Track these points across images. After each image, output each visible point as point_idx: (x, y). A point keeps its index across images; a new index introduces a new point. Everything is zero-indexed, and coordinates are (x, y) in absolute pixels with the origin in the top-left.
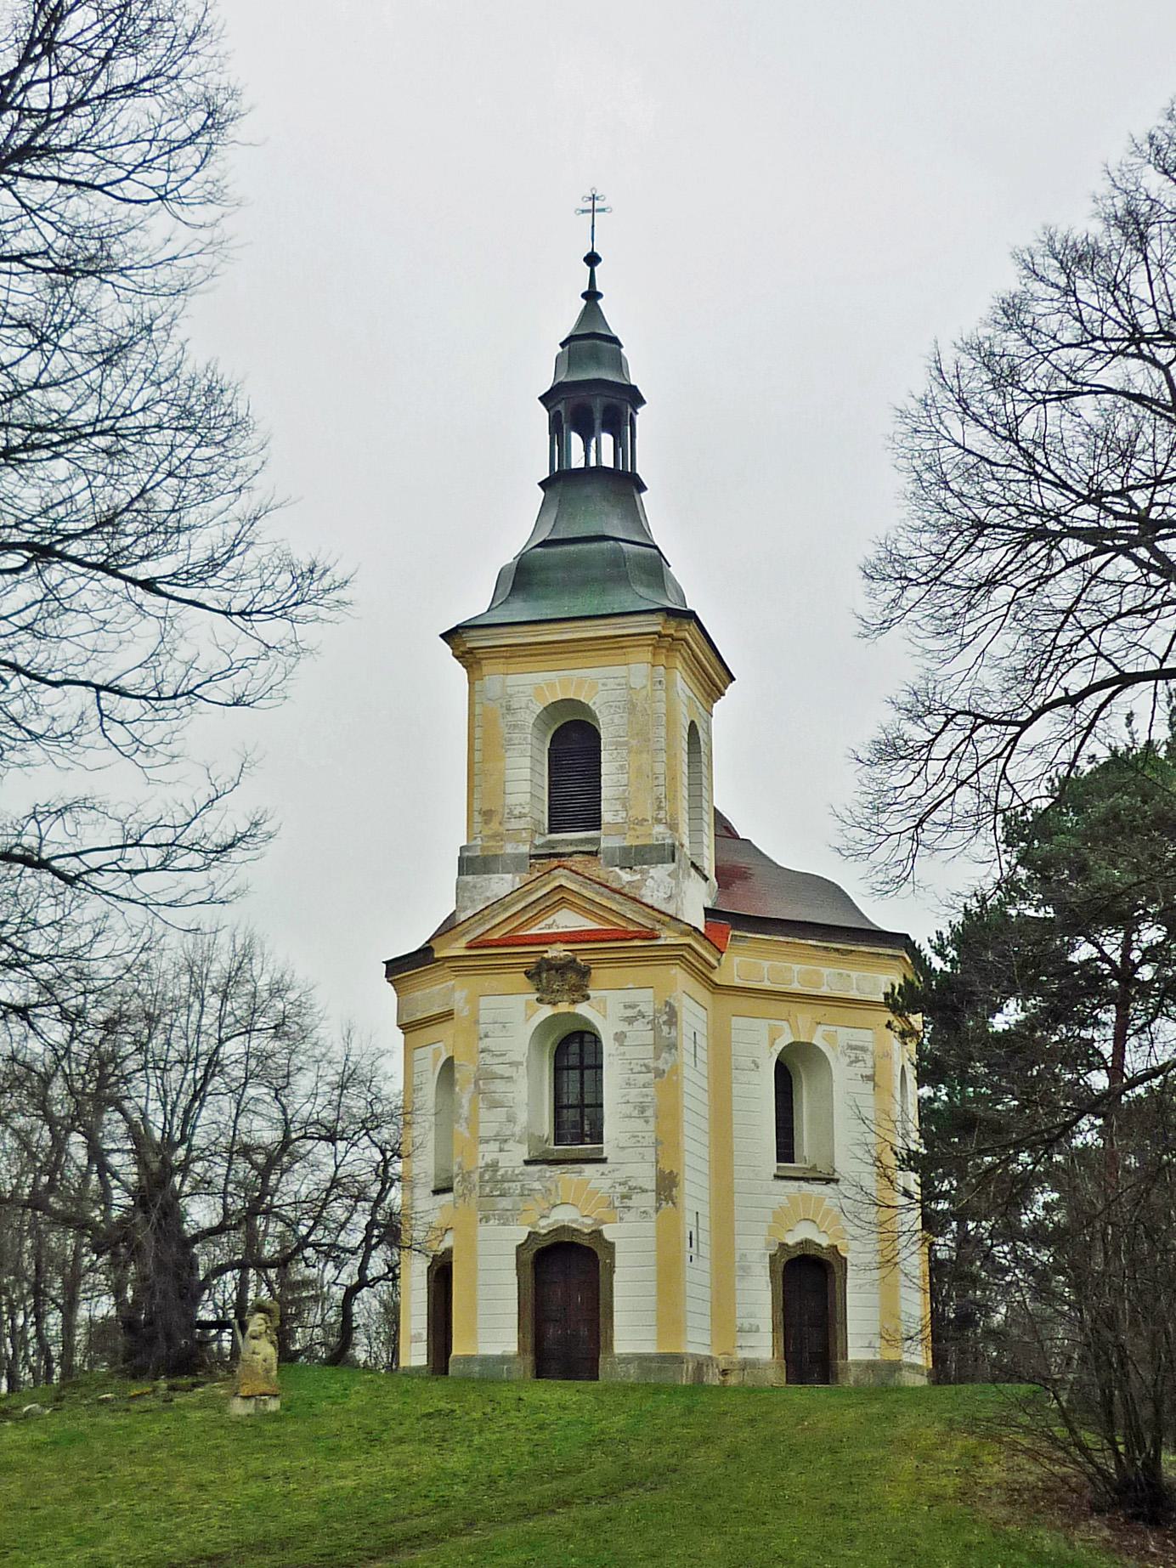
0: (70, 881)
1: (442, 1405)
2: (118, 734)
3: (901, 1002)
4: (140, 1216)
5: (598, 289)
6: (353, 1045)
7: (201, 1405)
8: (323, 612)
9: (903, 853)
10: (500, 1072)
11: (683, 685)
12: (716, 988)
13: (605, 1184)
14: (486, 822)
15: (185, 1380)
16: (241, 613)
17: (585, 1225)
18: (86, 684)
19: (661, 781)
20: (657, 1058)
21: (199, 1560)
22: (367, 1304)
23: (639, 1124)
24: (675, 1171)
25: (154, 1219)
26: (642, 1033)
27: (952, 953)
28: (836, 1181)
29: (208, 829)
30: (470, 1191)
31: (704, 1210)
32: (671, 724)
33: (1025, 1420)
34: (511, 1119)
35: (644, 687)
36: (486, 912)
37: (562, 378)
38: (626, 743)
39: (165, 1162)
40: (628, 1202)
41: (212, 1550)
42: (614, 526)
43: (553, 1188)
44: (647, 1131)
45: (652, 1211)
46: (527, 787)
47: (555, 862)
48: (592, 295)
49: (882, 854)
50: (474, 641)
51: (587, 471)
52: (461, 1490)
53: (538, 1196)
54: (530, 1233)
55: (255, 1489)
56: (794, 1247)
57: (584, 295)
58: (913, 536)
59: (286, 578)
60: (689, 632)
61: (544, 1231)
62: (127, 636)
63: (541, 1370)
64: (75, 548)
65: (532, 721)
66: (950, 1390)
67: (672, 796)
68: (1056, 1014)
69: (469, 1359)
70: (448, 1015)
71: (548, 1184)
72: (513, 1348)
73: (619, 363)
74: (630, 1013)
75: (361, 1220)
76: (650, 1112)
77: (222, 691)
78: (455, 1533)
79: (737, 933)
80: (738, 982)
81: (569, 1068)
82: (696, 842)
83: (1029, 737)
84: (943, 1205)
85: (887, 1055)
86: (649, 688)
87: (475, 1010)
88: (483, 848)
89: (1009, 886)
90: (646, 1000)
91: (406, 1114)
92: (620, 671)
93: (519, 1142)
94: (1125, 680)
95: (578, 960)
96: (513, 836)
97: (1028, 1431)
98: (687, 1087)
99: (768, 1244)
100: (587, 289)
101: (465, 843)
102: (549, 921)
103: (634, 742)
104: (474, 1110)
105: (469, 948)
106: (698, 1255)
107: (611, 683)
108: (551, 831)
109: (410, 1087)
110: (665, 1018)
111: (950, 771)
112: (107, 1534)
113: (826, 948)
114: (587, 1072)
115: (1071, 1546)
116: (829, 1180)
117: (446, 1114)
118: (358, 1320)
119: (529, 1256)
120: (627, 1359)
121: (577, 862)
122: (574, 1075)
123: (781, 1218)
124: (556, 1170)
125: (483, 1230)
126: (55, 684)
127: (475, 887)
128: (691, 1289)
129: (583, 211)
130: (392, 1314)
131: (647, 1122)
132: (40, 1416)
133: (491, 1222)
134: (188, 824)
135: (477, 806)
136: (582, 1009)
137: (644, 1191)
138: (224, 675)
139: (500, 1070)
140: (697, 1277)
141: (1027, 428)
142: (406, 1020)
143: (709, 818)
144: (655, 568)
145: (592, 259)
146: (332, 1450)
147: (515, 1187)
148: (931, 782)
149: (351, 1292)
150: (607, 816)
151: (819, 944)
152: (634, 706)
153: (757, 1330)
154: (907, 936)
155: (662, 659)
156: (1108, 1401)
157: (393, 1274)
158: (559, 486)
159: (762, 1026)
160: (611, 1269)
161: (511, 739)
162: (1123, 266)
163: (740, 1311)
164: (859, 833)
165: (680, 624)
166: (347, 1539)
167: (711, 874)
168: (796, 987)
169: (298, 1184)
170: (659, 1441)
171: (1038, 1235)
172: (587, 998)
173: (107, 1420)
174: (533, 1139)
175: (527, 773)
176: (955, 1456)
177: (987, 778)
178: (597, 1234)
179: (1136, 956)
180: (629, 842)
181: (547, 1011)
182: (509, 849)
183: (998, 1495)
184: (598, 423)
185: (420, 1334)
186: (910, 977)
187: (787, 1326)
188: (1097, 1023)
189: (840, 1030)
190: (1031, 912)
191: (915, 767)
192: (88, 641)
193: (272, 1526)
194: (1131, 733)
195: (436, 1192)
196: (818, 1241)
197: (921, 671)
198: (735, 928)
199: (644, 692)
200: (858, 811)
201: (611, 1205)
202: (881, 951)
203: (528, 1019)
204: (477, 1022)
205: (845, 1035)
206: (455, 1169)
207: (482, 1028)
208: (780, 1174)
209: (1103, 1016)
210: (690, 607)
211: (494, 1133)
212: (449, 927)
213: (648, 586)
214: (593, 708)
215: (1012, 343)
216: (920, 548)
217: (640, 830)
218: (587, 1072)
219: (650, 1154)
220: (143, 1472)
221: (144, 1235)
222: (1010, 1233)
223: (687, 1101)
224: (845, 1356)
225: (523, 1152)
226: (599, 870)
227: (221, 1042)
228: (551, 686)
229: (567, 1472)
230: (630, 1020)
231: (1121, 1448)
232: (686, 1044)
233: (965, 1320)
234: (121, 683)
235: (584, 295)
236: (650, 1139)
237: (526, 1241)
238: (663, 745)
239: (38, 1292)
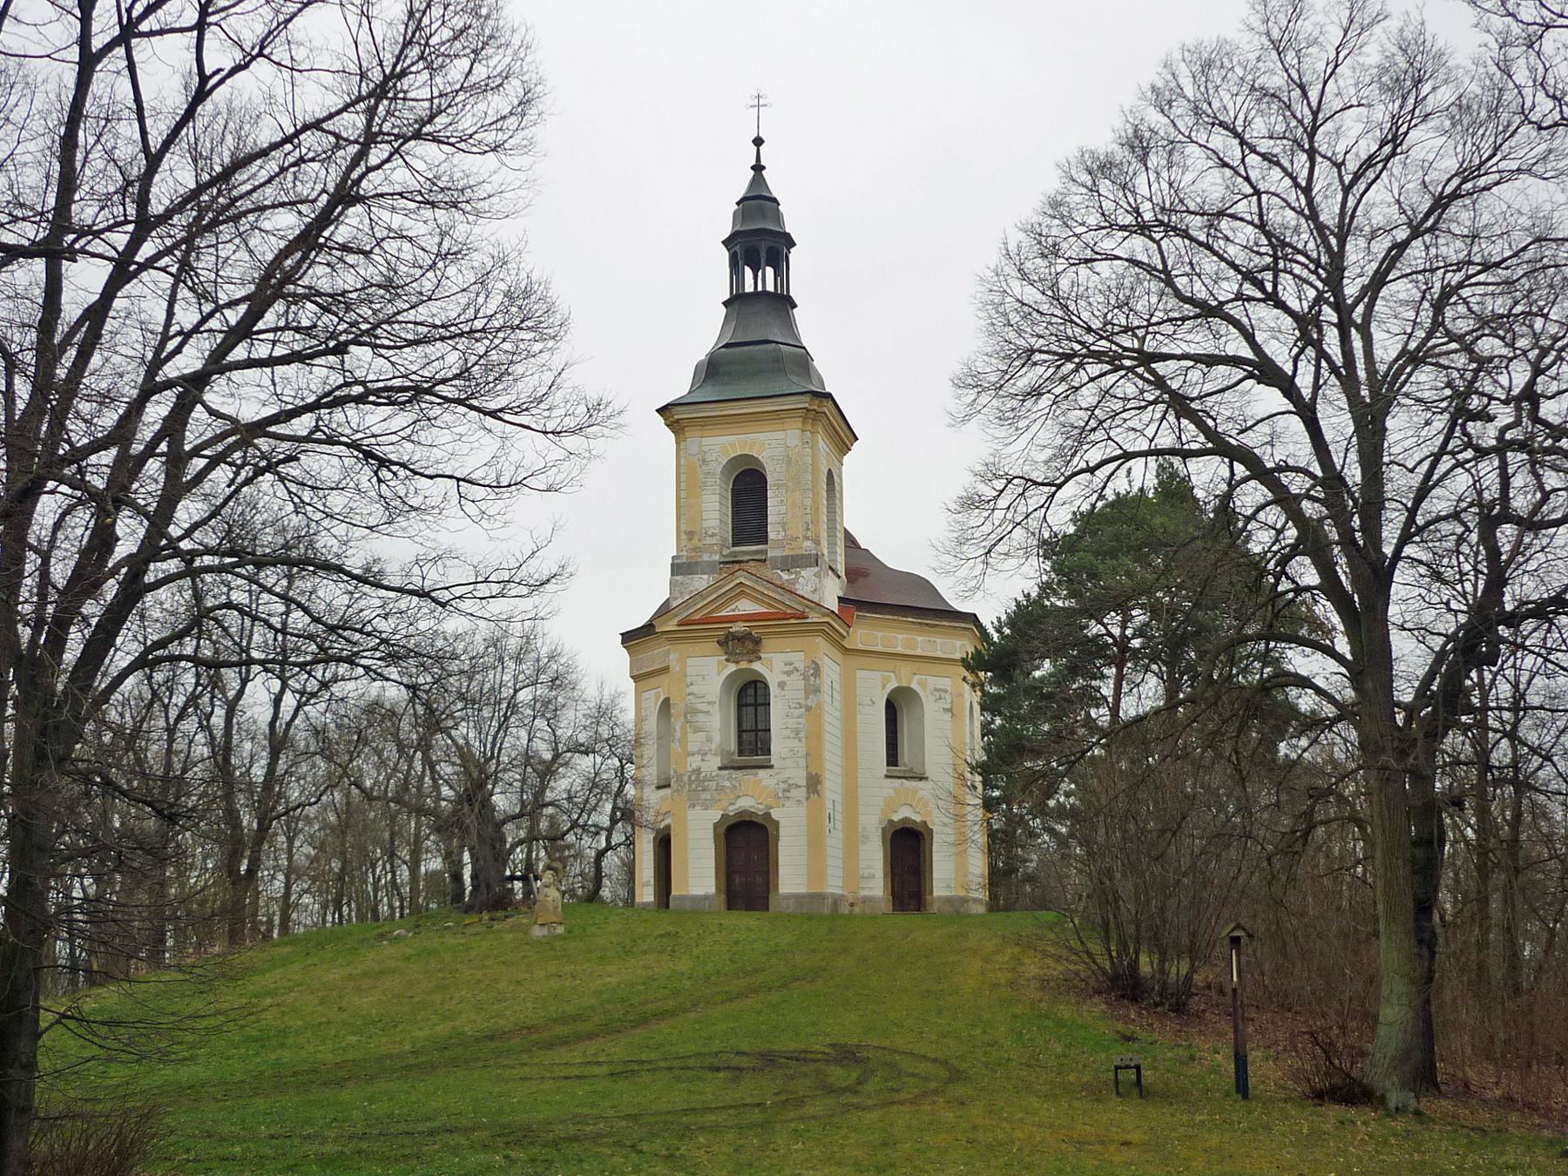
0: (443, 605)
1: (670, 929)
2: (470, 508)
3: (974, 664)
4: (466, 808)
5: (763, 163)
6: (605, 693)
7: (511, 930)
8: (606, 432)
9: (977, 571)
11: (823, 444)
12: (847, 651)
14: (690, 540)
15: (500, 914)
16: (552, 433)
17: (759, 809)
18: (451, 477)
20: (807, 698)
21: (522, 1028)
22: (611, 861)
23: (794, 743)
25: (476, 810)
26: (796, 682)
27: (1007, 631)
28: (926, 779)
29: (532, 570)
31: (839, 799)
32: (815, 471)
33: (1052, 936)
34: (709, 740)
38: (785, 485)
39: (482, 771)
40: (788, 794)
41: (529, 1023)
44: (801, 748)
45: (804, 800)
47: (737, 566)
48: (758, 168)
49: (963, 572)
50: (680, 414)
51: (756, 294)
52: (688, 984)
55: (554, 984)
57: (752, 168)
58: (986, 358)
59: (582, 409)
62: (476, 445)
63: (731, 906)
64: (442, 389)
66: (1002, 916)
67: (816, 521)
68: (1074, 670)
69: (682, 898)
70: (666, 670)
72: (713, 890)
73: (777, 217)
75: (608, 807)
76: (802, 735)
77: (539, 482)
78: (686, 1011)
80: (860, 647)
81: (747, 705)
82: (833, 552)
83: (1062, 494)
84: (996, 793)
85: (961, 695)
87: (684, 667)
89: (1046, 589)
90: (799, 660)
91: (638, 742)
92: (780, 435)
94: (1127, 456)
97: (1055, 944)
98: (827, 718)
102: (733, 607)
104: (684, 733)
108: (734, 545)
109: (640, 720)
111: (1009, 516)
112: (460, 1013)
115: (1081, 1015)
117: (665, 736)
118: (605, 871)
119: (722, 830)
120: (789, 897)
121: (751, 566)
122: (752, 709)
124: (740, 773)
126: (431, 477)
130: (630, 869)
132: (405, 937)
134: (519, 568)
136: (756, 666)
137: (798, 786)
138: (543, 470)
140: (834, 843)
141: (1064, 284)
142: (636, 673)
143: (840, 536)
144: (803, 362)
145: (758, 142)
146: (601, 958)
147: (713, 785)
148: (997, 524)
149: (600, 854)
150: (771, 535)
152: (789, 460)
153: (873, 877)
154: (975, 615)
156: (1106, 924)
157: (630, 843)
158: (737, 304)
159: (877, 676)
162: (1131, 173)
163: (862, 865)
164: (948, 558)
166: (616, 1016)
167: (843, 574)
168: (900, 650)
169: (560, 786)
170: (813, 951)
171: (1061, 813)
173: (450, 940)
174: (724, 753)
176: (1006, 959)
177: (1033, 524)
178: (767, 815)
179: (1129, 632)
181: (732, 668)
182: (706, 557)
183: (1034, 984)
184: (763, 260)
186: (979, 647)
187: (893, 874)
188: (1103, 677)
190: (1060, 604)
191: (986, 514)
192: (449, 448)
193: (567, 1008)
194: (1130, 482)
195: (658, 788)
197: (991, 451)
200: (947, 543)
201: (776, 796)
204: (685, 675)
205: (932, 682)
206: (672, 773)
207: (689, 680)
209: (1106, 671)
210: (828, 390)
212: (664, 610)
213: (798, 375)
215: (1055, 229)
216: (990, 369)
219: (802, 762)
220: (479, 974)
221: (470, 820)
222: (1040, 810)
223: (828, 727)
225: (717, 761)
226: (767, 572)
227: (516, 691)
228: (732, 445)
229: (755, 971)
231: (1114, 954)
232: (826, 688)
233: (1010, 870)
234: (473, 476)
235: (752, 168)
239: (392, 855)
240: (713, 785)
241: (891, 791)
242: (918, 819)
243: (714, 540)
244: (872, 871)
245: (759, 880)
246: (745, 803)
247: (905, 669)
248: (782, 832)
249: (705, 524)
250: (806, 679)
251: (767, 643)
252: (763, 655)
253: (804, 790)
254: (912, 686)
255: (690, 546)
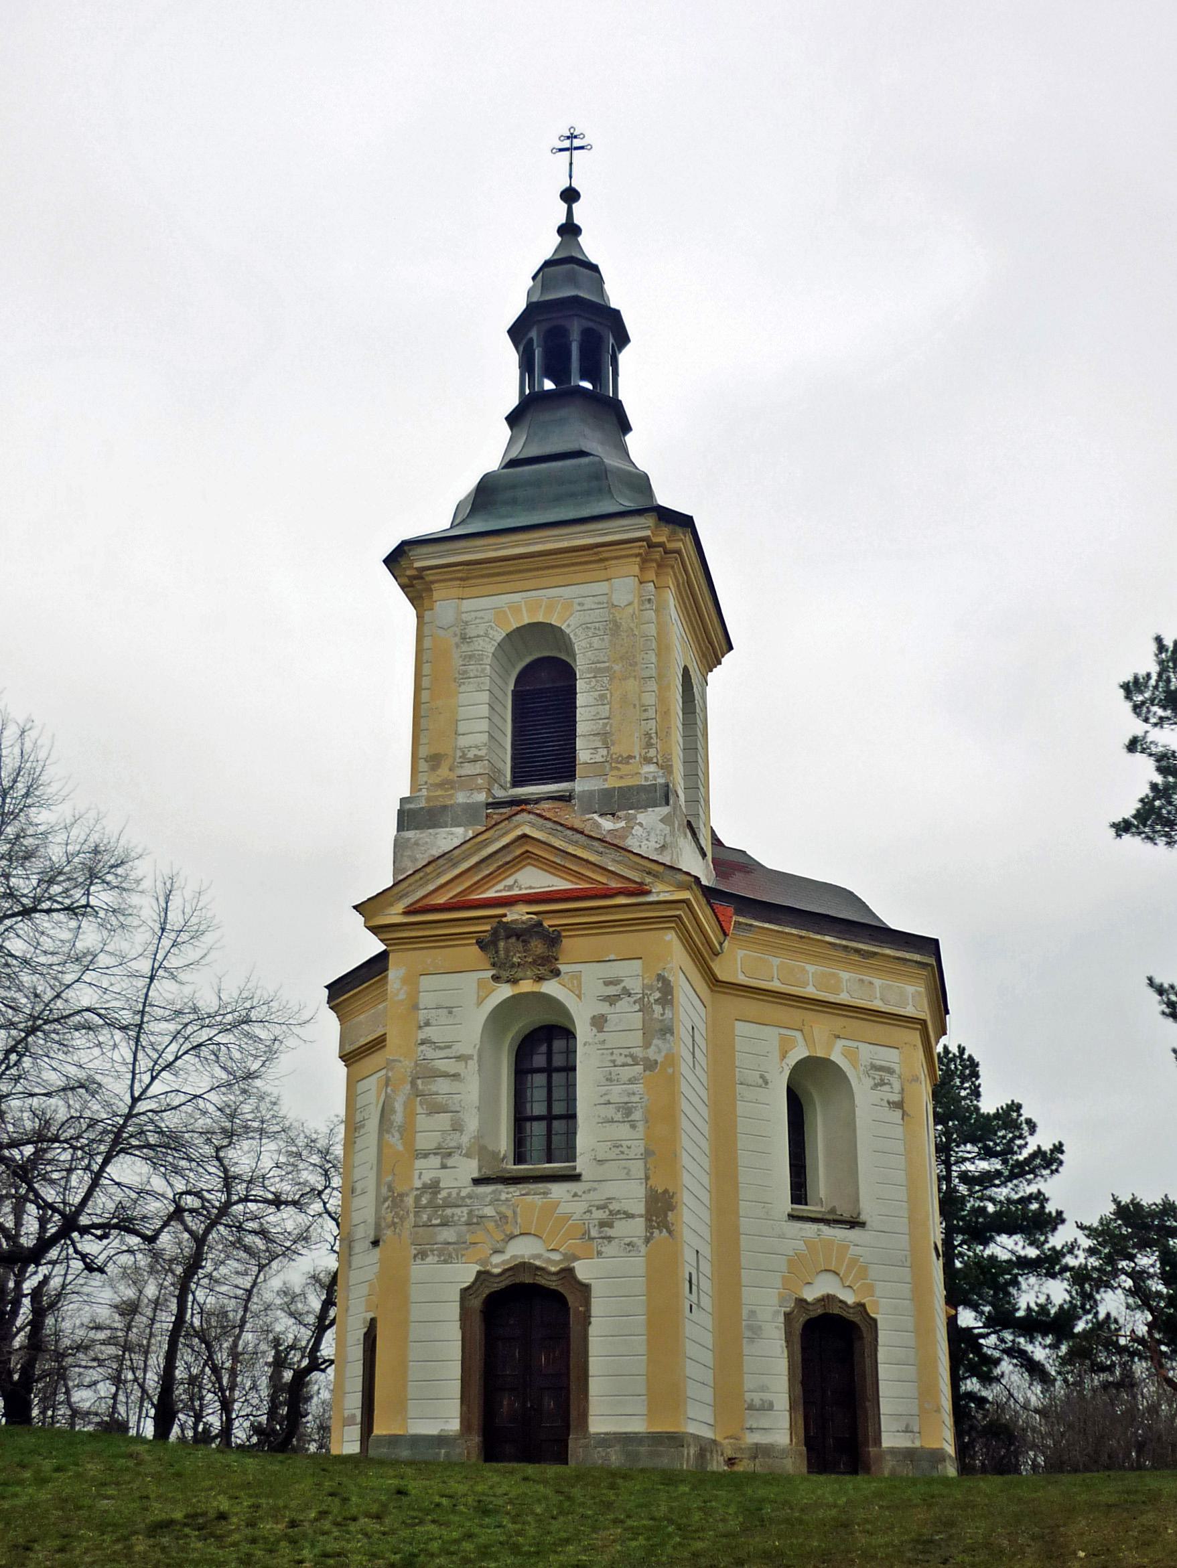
10: (443, 1069)
13: (578, 1208)
14: (434, 768)
17: (552, 1261)
19: (651, 714)
20: (647, 1045)
23: (623, 1131)
24: (671, 1191)
26: (627, 1015)
28: (862, 1225)
30: (402, 1219)
31: (706, 1251)
34: (457, 1127)
35: (630, 604)
36: (428, 869)
37: (534, 299)
38: (608, 669)
42: (594, 443)
43: (509, 1213)
44: (633, 1138)
45: (639, 1242)
46: (484, 725)
48: (569, 230)
53: (491, 1225)
54: (479, 1273)
56: (813, 1304)
60: (682, 543)
61: (497, 1271)
65: (493, 650)
71: (503, 1209)
72: (454, 1426)
74: (612, 990)
79: (741, 920)
80: (742, 979)
86: (636, 605)
88: (428, 799)
90: (632, 974)
92: (603, 587)
93: (468, 1155)
95: (546, 924)
96: (466, 782)
99: (782, 1300)
100: (564, 221)
101: (408, 794)
102: (510, 881)
103: (617, 667)
104: (410, 1115)
105: (408, 912)
106: (698, 1305)
107: (589, 604)
108: (516, 783)
110: (657, 995)
113: (846, 947)
114: (555, 1076)
116: (855, 1223)
119: (476, 1303)
120: (607, 1440)
123: (799, 1267)
124: (514, 1191)
125: (418, 1270)
127: (417, 844)
128: (691, 1349)
129: (561, 150)
131: (633, 1127)
133: (429, 1259)
135: (424, 752)
136: (551, 988)
137: (630, 1216)
139: (443, 1065)
142: (348, 1049)
145: (570, 196)
147: (462, 1213)
150: (584, 754)
151: (838, 941)
153: (771, 1407)
155: (651, 575)
159: (771, 1035)
160: (586, 1319)
161: (465, 672)
163: (749, 1382)
165: (674, 533)
168: (810, 991)
172: (556, 973)
174: (482, 1151)
175: (484, 710)
180: (612, 783)
181: (505, 992)
182: (461, 798)
185: (354, 1416)
187: (807, 1403)
189: (862, 1046)
196: (841, 1298)
198: (739, 912)
199: (630, 610)
201: (586, 1236)
202: (908, 956)
203: (480, 1002)
204: (416, 1007)
205: (866, 1053)
207: (422, 1015)
208: (795, 1213)
211: (434, 1145)
214: (567, 631)
217: (625, 769)
218: (555, 1076)
219: (638, 1168)
224: (878, 1441)
225: (470, 1168)
228: (516, 609)
230: (611, 1000)
232: (683, 1032)
236: (638, 1148)
237: (474, 1283)
238: (654, 673)
240: (462, 1213)
241: (800, 1245)
242: (850, 1298)
243: (477, 768)
244: (767, 1396)
245: (550, 1404)
246: (524, 1250)
247: (822, 1026)
248: (598, 1307)
249: (463, 742)
250: (645, 1009)
251: (571, 945)
252: (562, 968)
253: (640, 1222)
254: (832, 1058)
255: (434, 779)
